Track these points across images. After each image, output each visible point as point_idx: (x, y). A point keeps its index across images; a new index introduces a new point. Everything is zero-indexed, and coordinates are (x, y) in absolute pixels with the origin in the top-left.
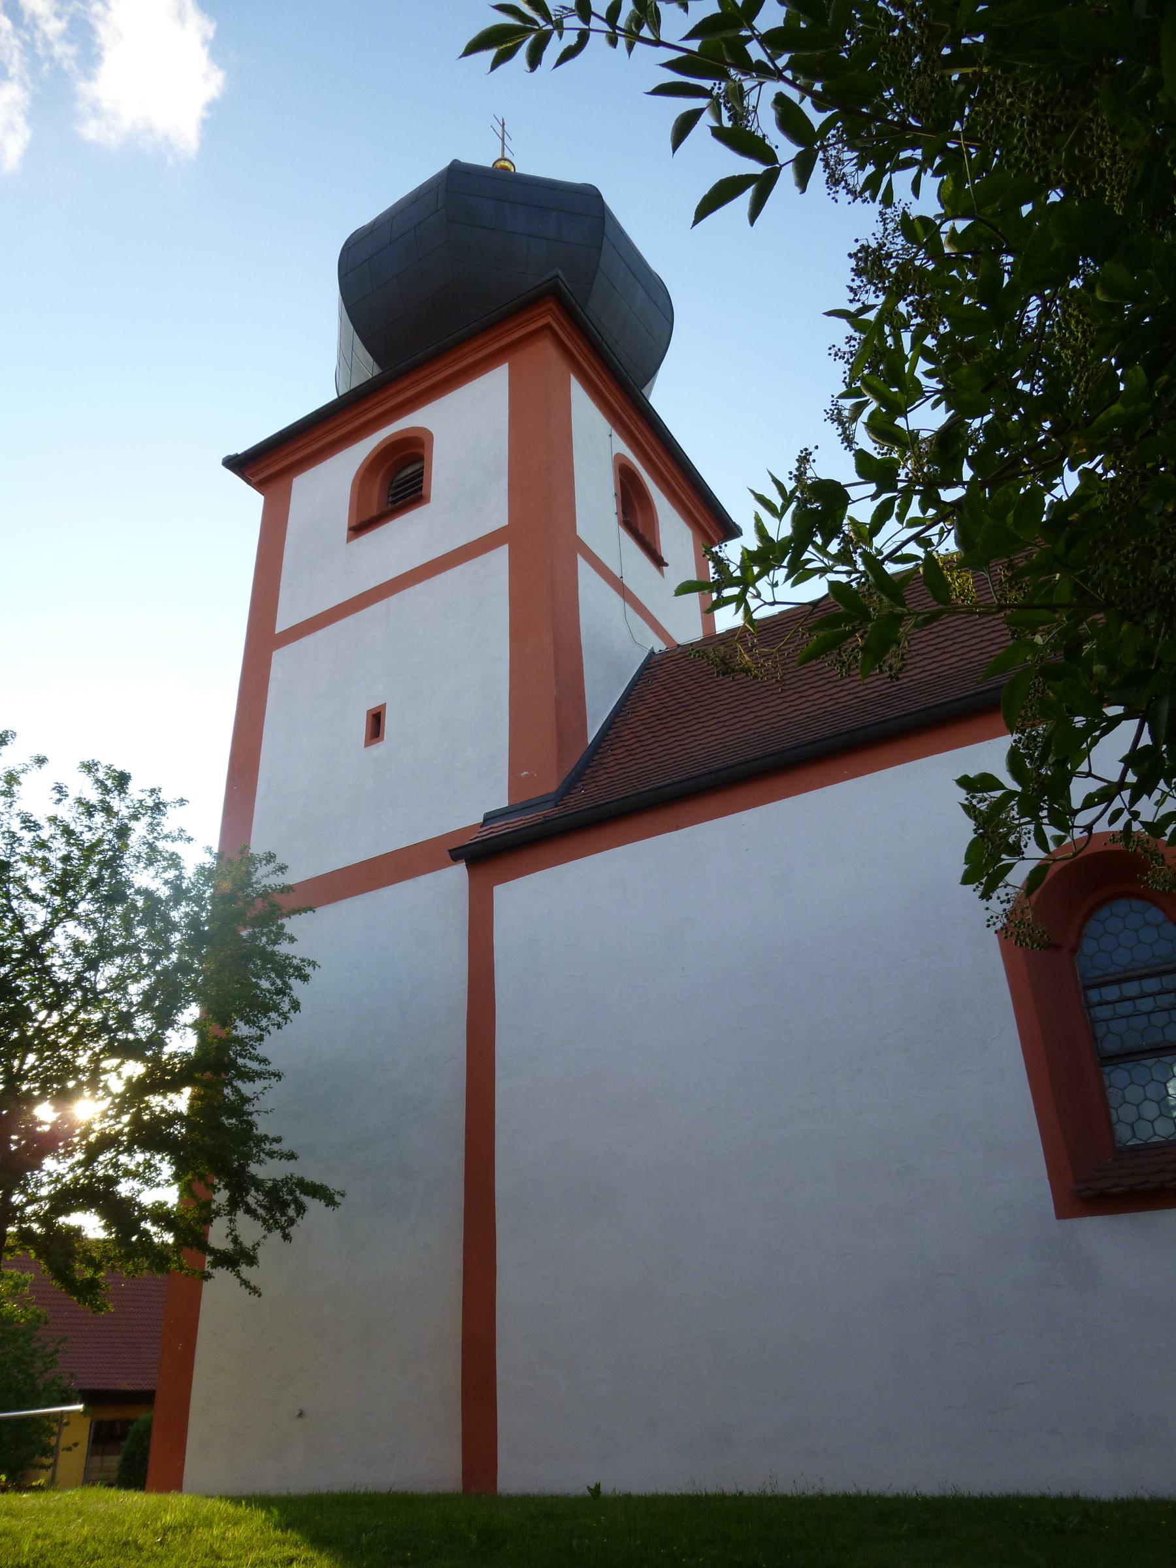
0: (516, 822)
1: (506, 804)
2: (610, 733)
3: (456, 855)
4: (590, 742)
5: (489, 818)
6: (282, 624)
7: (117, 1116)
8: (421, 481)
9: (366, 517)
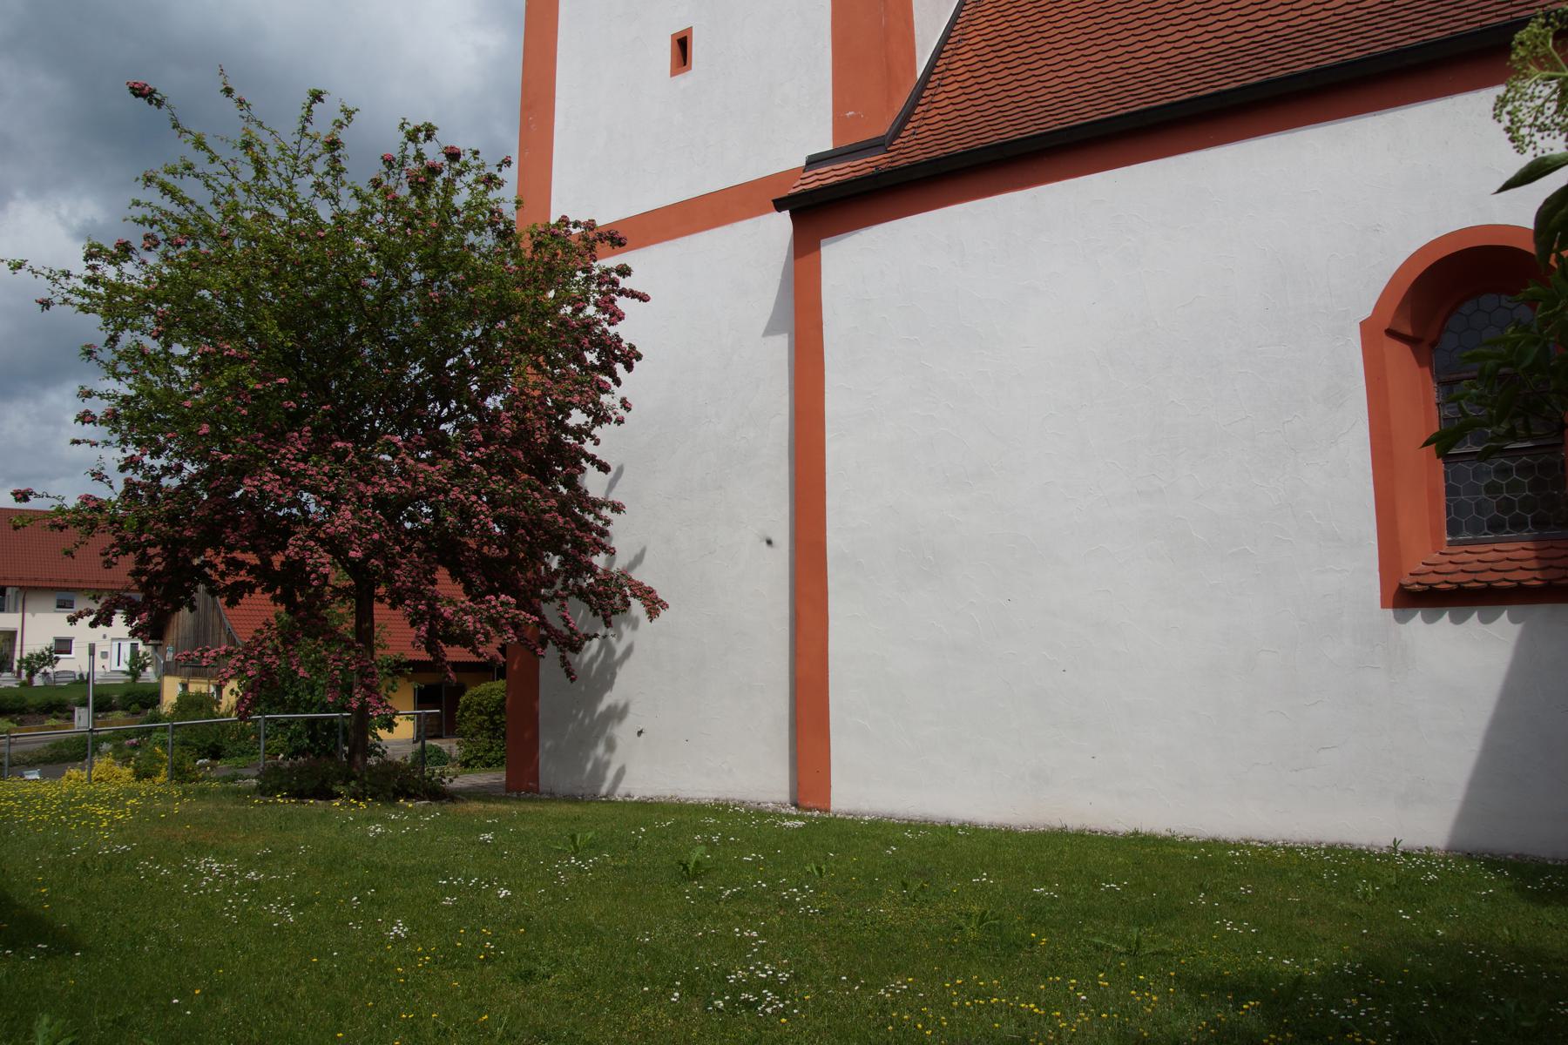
0: (830, 175)
1: (830, 147)
2: (938, 64)
3: (779, 205)
4: (919, 76)
5: (814, 161)
7: (338, 568)
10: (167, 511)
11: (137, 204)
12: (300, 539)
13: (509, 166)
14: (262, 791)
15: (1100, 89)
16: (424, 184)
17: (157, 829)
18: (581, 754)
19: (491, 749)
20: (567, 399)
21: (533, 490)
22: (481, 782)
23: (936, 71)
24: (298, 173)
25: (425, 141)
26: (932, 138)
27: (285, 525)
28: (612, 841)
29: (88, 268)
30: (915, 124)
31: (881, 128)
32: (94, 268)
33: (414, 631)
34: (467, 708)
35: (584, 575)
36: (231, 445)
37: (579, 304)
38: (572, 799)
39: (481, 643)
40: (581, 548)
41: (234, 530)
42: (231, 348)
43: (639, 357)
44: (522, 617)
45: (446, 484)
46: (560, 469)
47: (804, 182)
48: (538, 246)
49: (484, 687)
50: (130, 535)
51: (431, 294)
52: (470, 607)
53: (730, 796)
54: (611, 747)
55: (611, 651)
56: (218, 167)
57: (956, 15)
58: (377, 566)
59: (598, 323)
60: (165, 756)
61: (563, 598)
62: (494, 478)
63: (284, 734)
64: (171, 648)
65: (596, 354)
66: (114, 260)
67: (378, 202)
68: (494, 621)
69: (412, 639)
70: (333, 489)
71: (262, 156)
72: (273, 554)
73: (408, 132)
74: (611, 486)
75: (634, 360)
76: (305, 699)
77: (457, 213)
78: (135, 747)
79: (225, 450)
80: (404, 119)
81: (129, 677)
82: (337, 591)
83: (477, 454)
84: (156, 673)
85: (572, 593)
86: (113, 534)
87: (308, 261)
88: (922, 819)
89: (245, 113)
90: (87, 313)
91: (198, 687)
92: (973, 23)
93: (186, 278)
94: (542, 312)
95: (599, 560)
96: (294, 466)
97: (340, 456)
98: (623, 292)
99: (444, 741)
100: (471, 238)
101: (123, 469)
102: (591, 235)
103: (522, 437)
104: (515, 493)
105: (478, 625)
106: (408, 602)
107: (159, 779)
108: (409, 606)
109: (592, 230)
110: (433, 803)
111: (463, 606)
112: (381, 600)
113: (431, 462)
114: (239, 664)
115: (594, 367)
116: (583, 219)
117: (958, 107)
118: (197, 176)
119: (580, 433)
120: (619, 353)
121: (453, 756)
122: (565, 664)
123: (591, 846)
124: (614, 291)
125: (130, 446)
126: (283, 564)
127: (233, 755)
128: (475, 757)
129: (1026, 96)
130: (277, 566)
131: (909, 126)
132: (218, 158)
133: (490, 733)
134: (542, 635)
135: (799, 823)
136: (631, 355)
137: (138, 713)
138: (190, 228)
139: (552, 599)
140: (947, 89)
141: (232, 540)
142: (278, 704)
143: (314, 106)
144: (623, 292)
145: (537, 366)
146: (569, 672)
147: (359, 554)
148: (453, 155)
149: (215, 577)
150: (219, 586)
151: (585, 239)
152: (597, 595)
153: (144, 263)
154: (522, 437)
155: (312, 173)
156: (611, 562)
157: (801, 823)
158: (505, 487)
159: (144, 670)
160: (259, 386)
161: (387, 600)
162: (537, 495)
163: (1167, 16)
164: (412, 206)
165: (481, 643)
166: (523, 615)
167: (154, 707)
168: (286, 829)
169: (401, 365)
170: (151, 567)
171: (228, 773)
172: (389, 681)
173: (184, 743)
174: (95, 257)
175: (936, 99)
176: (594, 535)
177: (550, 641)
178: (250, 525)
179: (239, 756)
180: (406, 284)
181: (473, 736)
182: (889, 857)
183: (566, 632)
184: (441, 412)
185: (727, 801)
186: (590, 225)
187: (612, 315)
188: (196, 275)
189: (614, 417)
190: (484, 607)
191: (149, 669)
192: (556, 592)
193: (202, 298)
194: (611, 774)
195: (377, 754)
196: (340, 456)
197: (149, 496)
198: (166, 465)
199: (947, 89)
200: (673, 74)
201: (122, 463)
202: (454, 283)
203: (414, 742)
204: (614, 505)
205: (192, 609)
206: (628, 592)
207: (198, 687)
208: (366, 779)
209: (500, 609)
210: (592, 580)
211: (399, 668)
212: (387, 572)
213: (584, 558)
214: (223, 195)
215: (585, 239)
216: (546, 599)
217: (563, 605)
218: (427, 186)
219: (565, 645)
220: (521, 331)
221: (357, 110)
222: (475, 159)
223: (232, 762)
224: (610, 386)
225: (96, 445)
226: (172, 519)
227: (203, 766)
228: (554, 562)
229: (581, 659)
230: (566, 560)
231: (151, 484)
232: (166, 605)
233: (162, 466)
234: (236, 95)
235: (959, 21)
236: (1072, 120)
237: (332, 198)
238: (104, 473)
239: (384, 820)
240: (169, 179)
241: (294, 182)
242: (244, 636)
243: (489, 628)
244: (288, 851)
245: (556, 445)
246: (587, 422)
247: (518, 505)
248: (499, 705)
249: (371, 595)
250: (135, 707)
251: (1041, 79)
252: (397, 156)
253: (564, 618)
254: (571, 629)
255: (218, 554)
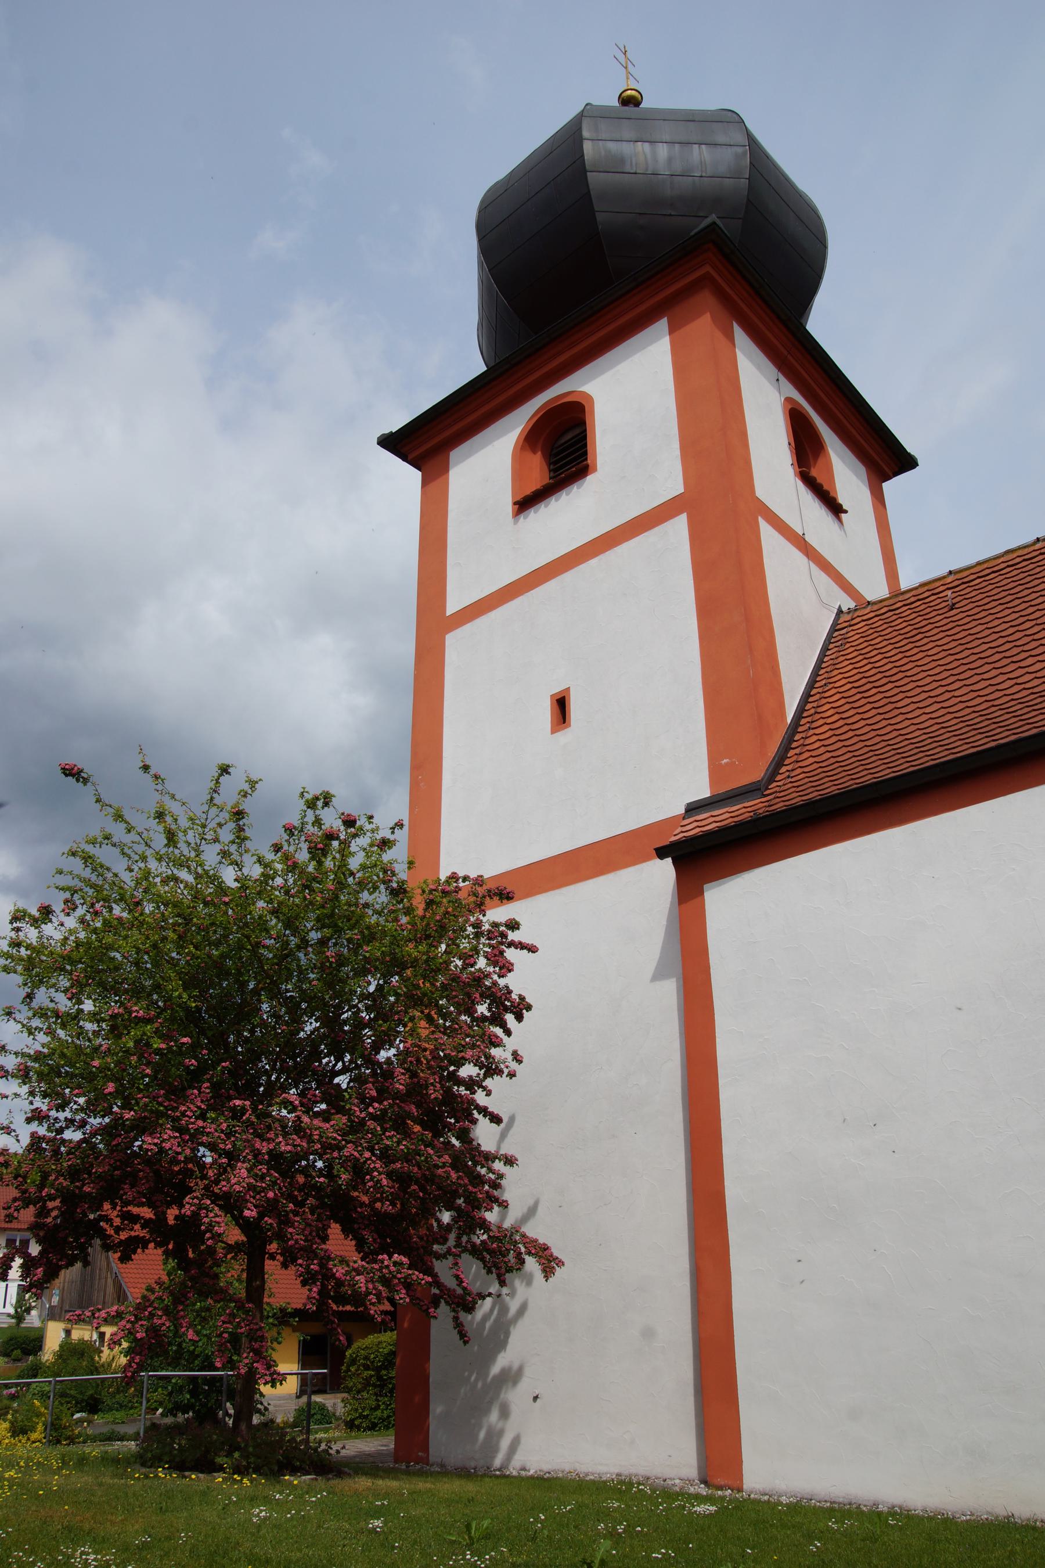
3: (661, 853)
4: (789, 720)
5: (693, 809)
6: (453, 605)
8: (585, 445)
9: (529, 490)
10: (69, 1166)
11: (60, 872)
12: (196, 1197)
13: (401, 828)
14: (146, 1460)
15: (967, 723)
16: (322, 849)
17: (34, 1508)
18: (473, 1421)
19: (377, 1408)
20: (461, 1055)
21: (426, 1146)
22: (367, 1449)
23: (805, 715)
24: (205, 840)
25: (323, 808)
26: (807, 780)
27: (180, 1179)
28: (509, 1530)
29: (13, 929)
30: (789, 768)
31: (757, 774)
32: (18, 930)
33: (305, 1291)
34: (353, 1361)
35: (478, 1232)
36: (133, 1102)
37: (469, 959)
38: (464, 1473)
39: (373, 1304)
40: (475, 1204)
41: (132, 1186)
42: (138, 1010)
43: (529, 1008)
44: (414, 1277)
45: (340, 1141)
46: (452, 1121)
47: (684, 829)
48: (430, 903)
49: (371, 1339)
50: (32, 1190)
51: (328, 954)
52: (363, 1266)
53: (633, 1471)
54: (505, 1413)
55: (504, 1309)
56: (133, 836)
57: (820, 661)
58: (271, 1224)
59: (488, 976)
60: (43, 1410)
61: (457, 1256)
62: (387, 1134)
63: (165, 1388)
64: (57, 1292)
65: (486, 1005)
66: (35, 922)
67: (279, 867)
68: (386, 1281)
69: (304, 1301)
70: (230, 1146)
71: (173, 827)
72: (168, 1208)
73: (307, 801)
74: (503, 1136)
75: (524, 1011)
76: (188, 1351)
77: (352, 874)
78: (13, 1397)
79: (126, 1106)
80: (304, 788)
81: (13, 1321)
82: (230, 1248)
83: (371, 1110)
84: (40, 1316)
85: (465, 1250)
86: (16, 1188)
87: (213, 924)
88: (846, 1501)
89: (160, 787)
90: (9, 973)
91: (82, 1333)
92: (838, 666)
93: (100, 941)
94: (432, 968)
95: (491, 1216)
96: (193, 1123)
97: (237, 1114)
98: (512, 944)
99: (328, 1396)
100: (365, 897)
101: (29, 1120)
102: (481, 891)
103: (416, 1091)
104: (408, 1148)
105: (371, 1286)
106: (300, 1261)
107: (34, 1436)
108: (301, 1265)
109: (481, 886)
110: (320, 1478)
111: (356, 1265)
112: (272, 1257)
113: (325, 1116)
114: (129, 1326)
115: (484, 1018)
116: (473, 875)
117: (829, 748)
118: (114, 845)
119: (472, 1084)
120: (509, 1004)
121: (338, 1414)
122: (459, 1325)
123: (487, 1536)
124: (502, 943)
125: (37, 1098)
126: (176, 1218)
127: (111, 1409)
128: (361, 1416)
129: (895, 733)
130: (171, 1221)
131: (783, 769)
132: (134, 828)
133: (377, 1390)
134: (435, 1294)
135: (711, 1508)
136: (521, 1006)
137: (18, 1360)
138: (105, 892)
139: (444, 1256)
140: (817, 731)
141: (129, 1196)
142: (160, 1356)
143: (222, 778)
144: (512, 944)
145: (430, 1020)
146: (463, 1335)
147: (254, 1214)
148: (349, 822)
149: (110, 1231)
150: (113, 1241)
151: (475, 895)
152: (492, 1252)
153: (62, 925)
154: (416, 1091)
155: (219, 842)
156: (503, 1217)
157: (713, 1508)
158: (399, 1143)
159: (29, 1313)
160: (164, 1046)
161: (279, 1257)
162: (430, 1151)
163: (1026, 648)
164: (311, 869)
165: (373, 1304)
166: (416, 1275)
167: (36, 1355)
168: (166, 1511)
169: (297, 1023)
170: (49, 1220)
171: (105, 1430)
172: (274, 1332)
173: (63, 1395)
174: (20, 920)
175: (808, 742)
176: (487, 1187)
177: (442, 1301)
178: (148, 1181)
179: (117, 1410)
180: (304, 943)
181: (359, 1392)
182: (813, 1554)
183: (459, 1291)
184: (335, 1065)
185: (630, 1475)
186: (479, 881)
187: (501, 968)
188: (109, 939)
189: (506, 1071)
190: (376, 1266)
191: (34, 1312)
192: (449, 1249)
193: (113, 958)
194: (505, 1444)
195: (259, 1411)
196: (237, 1114)
197: (53, 1151)
198: (69, 1117)
199: (817, 731)
200: (553, 731)
201: (29, 1115)
202: (349, 940)
203: (298, 1397)
204: (506, 1158)
205: (86, 1263)
206: (523, 1250)
207: (82, 1333)
208: (251, 1449)
209: (392, 1268)
210: (485, 1237)
211: (284, 1317)
212: (280, 1229)
213: (477, 1214)
214: (137, 861)
215: (475, 895)
216: (439, 1257)
217: (456, 1264)
218: (325, 852)
219: (458, 1305)
220: (414, 985)
221: (260, 780)
222: (370, 823)
223: (109, 1417)
224: (502, 1040)
225: (7, 1097)
226: (74, 1174)
227: (80, 1421)
228: (446, 1217)
229: (473, 1318)
230: (459, 1216)
231: (55, 1138)
232: (61, 1260)
233: (66, 1118)
234: (152, 771)
235: (824, 665)
236: (944, 756)
237: (237, 864)
238: (12, 1126)
239: (267, 1500)
240: (90, 849)
241: (202, 848)
242: (135, 1294)
243: (380, 1288)
244: (169, 1538)
245: (450, 1098)
246: (479, 1074)
247: (411, 1160)
248: (386, 1359)
249: (262, 1252)
250: (17, 1353)
251: (909, 716)
252: (297, 823)
253: (457, 1277)
254: (465, 1289)
255: (114, 1208)
